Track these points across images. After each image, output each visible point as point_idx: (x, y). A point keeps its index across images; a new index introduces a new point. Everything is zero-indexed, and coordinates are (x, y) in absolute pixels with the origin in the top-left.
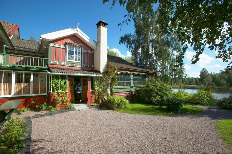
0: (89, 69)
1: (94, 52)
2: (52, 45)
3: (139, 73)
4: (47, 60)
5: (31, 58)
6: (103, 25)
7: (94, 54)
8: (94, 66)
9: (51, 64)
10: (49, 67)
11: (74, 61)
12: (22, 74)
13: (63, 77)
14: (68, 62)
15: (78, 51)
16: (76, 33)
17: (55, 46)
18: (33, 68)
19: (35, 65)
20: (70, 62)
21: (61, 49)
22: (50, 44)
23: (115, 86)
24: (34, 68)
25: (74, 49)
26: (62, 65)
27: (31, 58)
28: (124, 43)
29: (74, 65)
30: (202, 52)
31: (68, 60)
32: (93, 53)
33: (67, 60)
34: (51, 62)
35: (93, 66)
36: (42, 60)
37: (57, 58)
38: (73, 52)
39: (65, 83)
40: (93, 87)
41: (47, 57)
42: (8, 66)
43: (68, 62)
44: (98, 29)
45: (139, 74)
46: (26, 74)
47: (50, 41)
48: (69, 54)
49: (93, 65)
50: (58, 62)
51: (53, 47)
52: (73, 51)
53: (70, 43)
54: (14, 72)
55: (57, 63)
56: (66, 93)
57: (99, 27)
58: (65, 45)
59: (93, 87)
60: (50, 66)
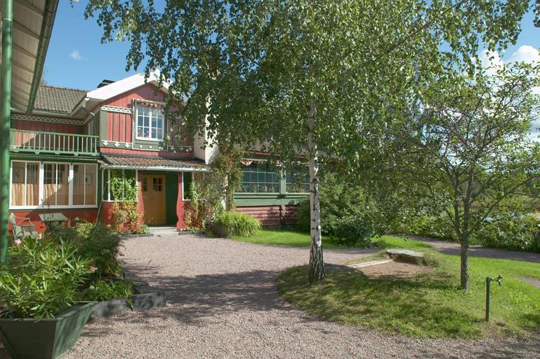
2: (106, 109)
4: (98, 139)
9: (105, 147)
13: (129, 174)
14: (138, 142)
17: (111, 110)
19: (76, 151)
21: (124, 115)
22: (102, 107)
23: (297, 192)
25: (151, 113)
26: (126, 149)
29: (151, 147)
31: (137, 138)
33: (135, 137)
34: (106, 143)
38: (147, 120)
39: (133, 184)
40: (188, 195)
43: (138, 143)
48: (140, 123)
51: (109, 112)
52: (152, 126)
55: (117, 144)
56: (135, 203)
58: (129, 106)
59: (188, 195)
60: (102, 150)
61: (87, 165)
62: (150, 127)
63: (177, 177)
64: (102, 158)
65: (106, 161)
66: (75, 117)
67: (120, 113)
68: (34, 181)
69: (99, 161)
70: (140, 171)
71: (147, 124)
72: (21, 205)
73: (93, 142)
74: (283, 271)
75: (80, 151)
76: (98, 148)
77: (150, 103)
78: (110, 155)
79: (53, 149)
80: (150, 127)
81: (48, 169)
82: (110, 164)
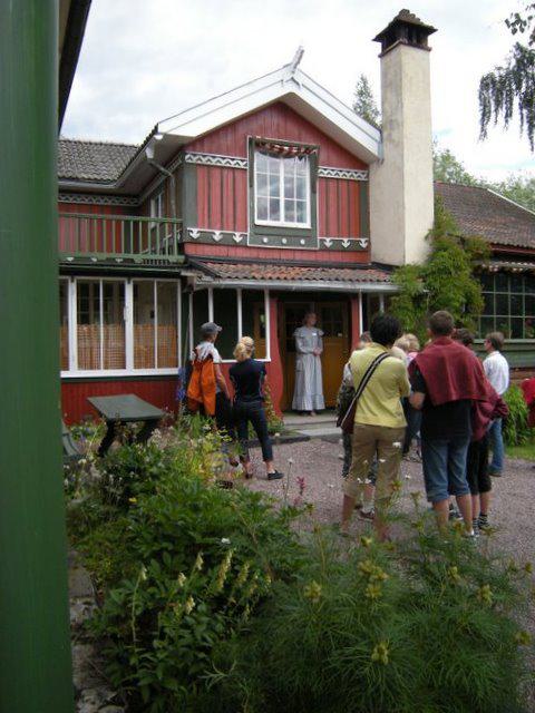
0: (347, 258)
1: (368, 176)
3: (502, 263)
4: (181, 225)
5: (114, 222)
6: (410, 38)
7: (366, 184)
8: (369, 242)
9: (195, 242)
10: (187, 256)
11: (282, 223)
12: (153, 283)
14: (261, 231)
15: (268, 174)
16: (291, 95)
18: (132, 260)
19: (119, 250)
20: (265, 231)
24: (136, 261)
26: (236, 245)
27: (114, 222)
28: (509, 115)
30: (210, 290)
31: (258, 222)
32: (363, 178)
33: (253, 221)
34: (195, 235)
35: (364, 245)
36: (136, 223)
37: (216, 218)
38: (275, 180)
41: (179, 214)
42: (70, 259)
43: (260, 231)
44: (388, 58)
45: (502, 270)
46: (108, 289)
47: (185, 142)
48: (301, 206)
49: (363, 240)
50: (218, 232)
52: (278, 201)
53: (264, 144)
54: (72, 281)
55: (217, 236)
57: (394, 53)
60: (190, 250)
61: (158, 283)
62: (282, 199)
63: (350, 304)
64: (189, 265)
65: (208, 273)
66: (121, 191)
67: (222, 168)
68: (115, 317)
69: (183, 273)
70: (275, 293)
71: (289, 206)
72: (124, 368)
73: (100, 227)
74: (467, 178)
75: (127, 251)
76: (181, 247)
77: (282, 144)
78: (214, 261)
79: (129, 252)
80: (282, 199)
81: (83, 291)
82: (217, 277)
